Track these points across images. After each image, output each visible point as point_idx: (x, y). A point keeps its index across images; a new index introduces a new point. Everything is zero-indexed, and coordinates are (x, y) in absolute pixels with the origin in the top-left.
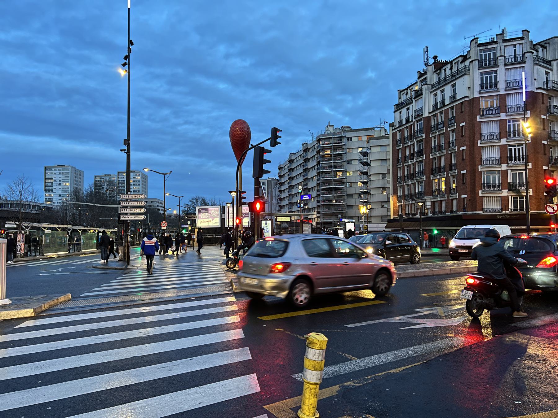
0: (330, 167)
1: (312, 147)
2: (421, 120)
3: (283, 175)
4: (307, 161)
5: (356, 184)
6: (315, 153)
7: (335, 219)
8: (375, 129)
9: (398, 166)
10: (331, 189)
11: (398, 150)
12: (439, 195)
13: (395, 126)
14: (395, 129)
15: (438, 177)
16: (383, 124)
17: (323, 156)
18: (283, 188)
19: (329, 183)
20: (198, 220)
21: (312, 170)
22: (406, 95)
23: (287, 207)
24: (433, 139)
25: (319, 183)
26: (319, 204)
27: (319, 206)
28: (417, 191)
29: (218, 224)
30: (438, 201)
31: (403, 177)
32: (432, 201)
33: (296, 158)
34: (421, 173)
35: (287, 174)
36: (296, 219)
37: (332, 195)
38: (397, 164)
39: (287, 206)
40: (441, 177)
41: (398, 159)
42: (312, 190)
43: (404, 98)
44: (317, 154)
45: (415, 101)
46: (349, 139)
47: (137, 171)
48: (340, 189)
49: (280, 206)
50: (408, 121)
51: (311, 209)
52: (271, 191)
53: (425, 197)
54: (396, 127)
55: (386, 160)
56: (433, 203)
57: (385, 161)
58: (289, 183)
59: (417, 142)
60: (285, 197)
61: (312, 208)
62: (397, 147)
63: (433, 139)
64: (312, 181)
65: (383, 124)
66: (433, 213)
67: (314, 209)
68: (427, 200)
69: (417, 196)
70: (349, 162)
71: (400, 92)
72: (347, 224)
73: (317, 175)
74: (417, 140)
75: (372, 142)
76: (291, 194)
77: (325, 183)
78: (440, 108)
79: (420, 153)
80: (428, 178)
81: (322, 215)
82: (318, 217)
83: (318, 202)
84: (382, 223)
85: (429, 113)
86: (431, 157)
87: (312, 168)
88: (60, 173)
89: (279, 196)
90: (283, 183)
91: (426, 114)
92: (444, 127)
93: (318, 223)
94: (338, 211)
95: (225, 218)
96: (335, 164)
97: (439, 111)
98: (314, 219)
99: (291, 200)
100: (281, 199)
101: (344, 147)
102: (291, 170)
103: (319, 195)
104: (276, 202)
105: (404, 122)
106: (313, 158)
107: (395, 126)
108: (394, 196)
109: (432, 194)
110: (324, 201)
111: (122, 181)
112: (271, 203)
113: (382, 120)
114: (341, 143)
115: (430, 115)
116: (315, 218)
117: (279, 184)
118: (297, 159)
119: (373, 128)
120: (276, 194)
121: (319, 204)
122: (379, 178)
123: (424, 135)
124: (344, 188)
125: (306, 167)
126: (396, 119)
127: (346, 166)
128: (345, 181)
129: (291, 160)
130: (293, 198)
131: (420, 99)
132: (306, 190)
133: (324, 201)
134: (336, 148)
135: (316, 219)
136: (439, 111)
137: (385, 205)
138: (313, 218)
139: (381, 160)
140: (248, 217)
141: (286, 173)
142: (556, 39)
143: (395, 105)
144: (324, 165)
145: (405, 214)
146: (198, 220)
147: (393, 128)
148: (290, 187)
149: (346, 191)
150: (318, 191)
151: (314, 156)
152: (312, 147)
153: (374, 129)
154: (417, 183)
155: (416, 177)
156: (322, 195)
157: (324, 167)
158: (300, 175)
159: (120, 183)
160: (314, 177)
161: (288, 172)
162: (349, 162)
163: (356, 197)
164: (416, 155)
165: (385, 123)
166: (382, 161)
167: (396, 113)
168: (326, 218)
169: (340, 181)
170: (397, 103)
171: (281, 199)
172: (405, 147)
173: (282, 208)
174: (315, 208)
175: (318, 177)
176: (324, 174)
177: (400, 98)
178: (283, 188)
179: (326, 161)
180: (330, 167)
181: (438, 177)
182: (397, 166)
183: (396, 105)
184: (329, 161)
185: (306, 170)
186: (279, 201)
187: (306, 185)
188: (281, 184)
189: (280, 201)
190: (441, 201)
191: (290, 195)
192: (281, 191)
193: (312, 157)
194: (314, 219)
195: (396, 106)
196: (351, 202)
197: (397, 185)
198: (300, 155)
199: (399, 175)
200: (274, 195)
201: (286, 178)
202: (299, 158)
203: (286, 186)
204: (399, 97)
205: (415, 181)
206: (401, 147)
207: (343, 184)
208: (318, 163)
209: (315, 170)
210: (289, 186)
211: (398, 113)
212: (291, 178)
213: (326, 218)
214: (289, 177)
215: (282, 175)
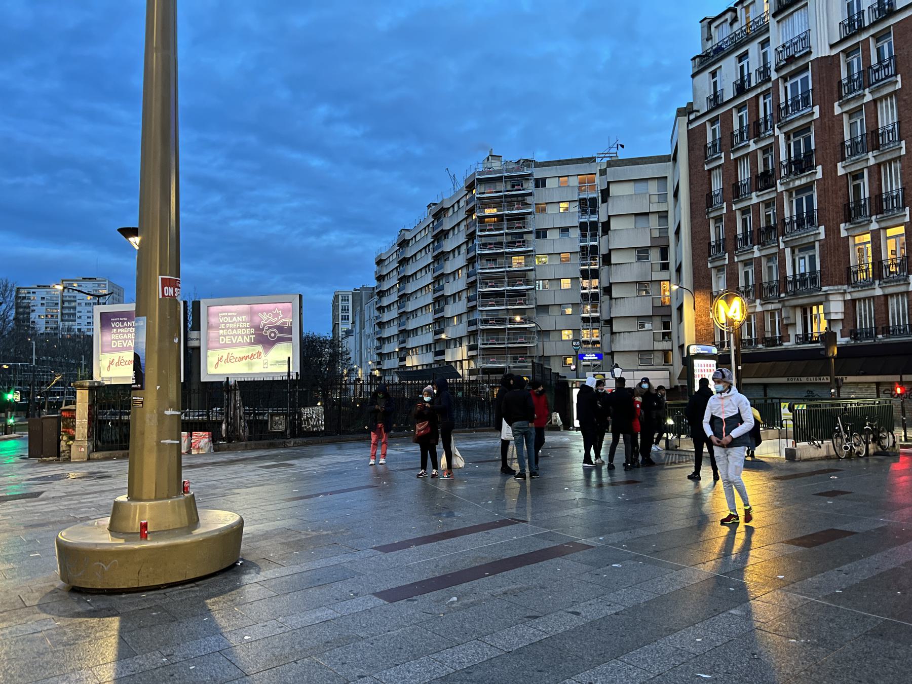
0: (499, 245)
1: (453, 206)
2: (805, 68)
3: (387, 274)
4: (441, 237)
5: (555, 282)
6: (462, 215)
7: (511, 362)
8: (598, 160)
9: (712, 215)
10: (500, 294)
11: (710, 171)
12: (880, 278)
13: (698, 111)
14: (697, 118)
15: (874, 226)
16: (614, 150)
17: (481, 219)
18: (385, 302)
19: (496, 279)
20: (101, 356)
21: (454, 255)
22: (731, 24)
23: (396, 340)
24: (845, 118)
25: (475, 281)
26: (473, 328)
27: (472, 334)
28: (789, 272)
29: (212, 370)
30: (873, 297)
31: (732, 242)
32: (848, 297)
33: (415, 236)
34: (804, 220)
35: (395, 272)
36: (415, 364)
37: (503, 308)
38: (708, 208)
39: (395, 337)
40: (883, 225)
41: (710, 197)
42: (413, 334)
43: (721, 35)
44: (466, 219)
45: (778, 22)
46: (541, 183)
47: (100, 279)
48: (522, 294)
49: (379, 339)
50: (741, 89)
51: (453, 341)
52: (362, 310)
53: (824, 289)
54: (699, 114)
55: (647, 214)
56: (850, 305)
57: (645, 218)
58: (399, 291)
59: (787, 136)
60: (390, 321)
61: (455, 339)
62: (733, 152)
63: (845, 118)
64: (454, 280)
65: (614, 150)
66: (854, 333)
67: (458, 341)
68: (831, 297)
69: (790, 287)
70: (541, 234)
71: (710, 23)
72: (696, 362)
73: (467, 266)
74: (786, 130)
75: (614, 173)
76: (404, 312)
77: (487, 279)
78: (872, 25)
79: (801, 164)
80: (832, 231)
81: (480, 353)
82: (471, 358)
83: (469, 326)
84: (640, 368)
85: (832, 46)
86: (841, 172)
87: (453, 251)
88: (88, 323)
89: (377, 318)
90: (387, 290)
91: (821, 50)
92: (896, 75)
93: (471, 372)
94: (519, 343)
95: (199, 348)
96: (510, 239)
97: (872, 31)
98: (458, 363)
99: (404, 325)
100: (381, 325)
101: (529, 200)
102: (404, 262)
103: (472, 309)
104: (372, 331)
105: (729, 94)
106: (456, 229)
107: (698, 111)
108: (697, 295)
109: (849, 279)
110: (485, 322)
111: (70, 297)
112: (361, 334)
113: (613, 141)
114: (524, 190)
115: (834, 52)
116: (461, 361)
117: (378, 293)
118: (418, 238)
119: (593, 158)
120: (372, 316)
121: (473, 328)
122: (632, 257)
123: (816, 109)
124: (530, 292)
125: (440, 250)
126: (699, 93)
127: (533, 243)
128: (531, 276)
129: (405, 240)
130: (409, 320)
131: (795, 14)
132: (441, 301)
133: (485, 322)
134: (511, 200)
135: (465, 364)
136: (872, 31)
137: (646, 325)
138: (456, 362)
139: (636, 215)
140: (290, 340)
141: (392, 271)
142: (1, 611)
143: (694, 59)
144: (484, 240)
145: (765, 338)
146: (101, 356)
147: (692, 117)
148: (401, 297)
149: (536, 299)
150: (469, 299)
151: (458, 224)
152: (453, 206)
153: (595, 161)
154: (788, 251)
155: (784, 235)
156: (481, 309)
157: (484, 246)
158: (424, 271)
159: (67, 301)
160: (458, 270)
161: (396, 268)
162: (541, 234)
163: (554, 311)
164: (784, 172)
165: (619, 146)
166: (639, 218)
167: (698, 78)
168: (491, 360)
169: (522, 276)
170: (700, 53)
171: (381, 325)
172: (736, 159)
173: (384, 343)
174: (461, 338)
175: (468, 269)
176: (484, 261)
177: (709, 38)
178: (385, 302)
179: (489, 230)
180: (499, 245)
181: (874, 226)
182: (708, 213)
183: (697, 56)
184: (496, 230)
185: (441, 257)
186: (377, 329)
187: (442, 288)
188: (381, 294)
189: (380, 328)
190: (886, 296)
191: (401, 314)
192: (381, 309)
193: (453, 228)
194: (458, 363)
195: (697, 60)
196: (546, 322)
197: (710, 266)
198: (425, 228)
199: (713, 239)
200: (367, 318)
201: (393, 280)
202: (423, 234)
203: (394, 297)
204: (706, 36)
205: (782, 246)
206: (723, 161)
207: (528, 282)
208: (471, 236)
209: (461, 256)
210: (399, 297)
211: (706, 74)
212: (404, 280)
213: (491, 360)
214: (400, 276)
215: (385, 275)
